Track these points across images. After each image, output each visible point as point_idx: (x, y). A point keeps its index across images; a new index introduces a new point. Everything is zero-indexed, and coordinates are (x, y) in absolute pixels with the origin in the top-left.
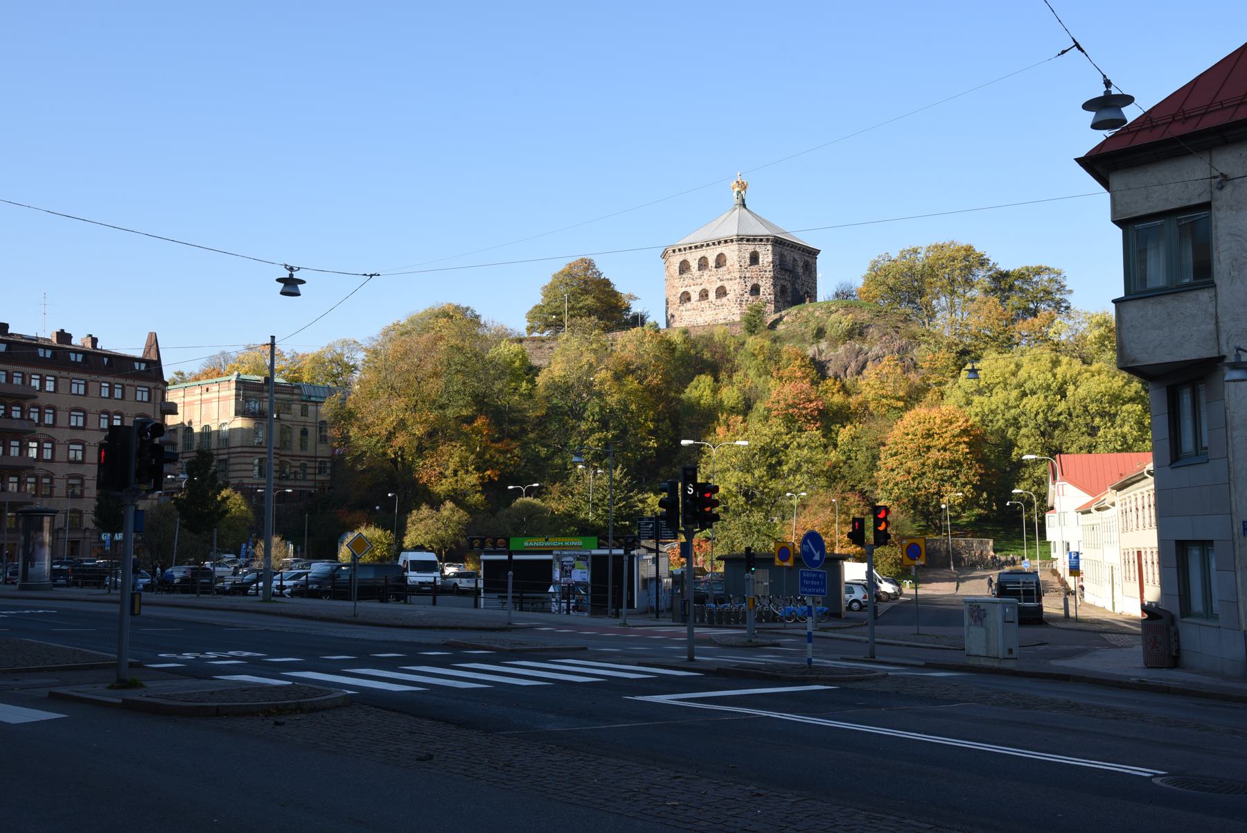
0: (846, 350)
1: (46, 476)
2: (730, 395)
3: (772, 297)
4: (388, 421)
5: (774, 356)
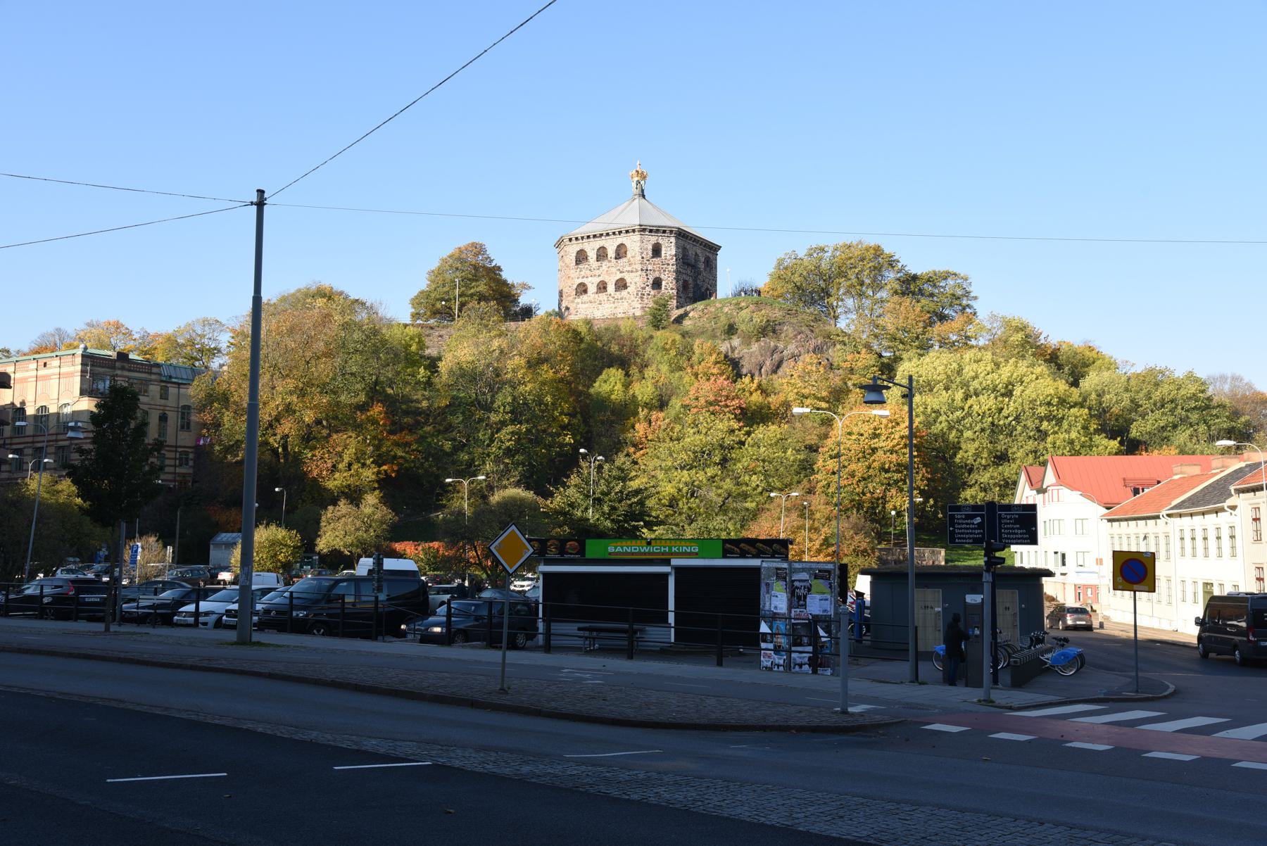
0: (761, 347)
2: (643, 390)
3: (675, 292)
5: (686, 352)
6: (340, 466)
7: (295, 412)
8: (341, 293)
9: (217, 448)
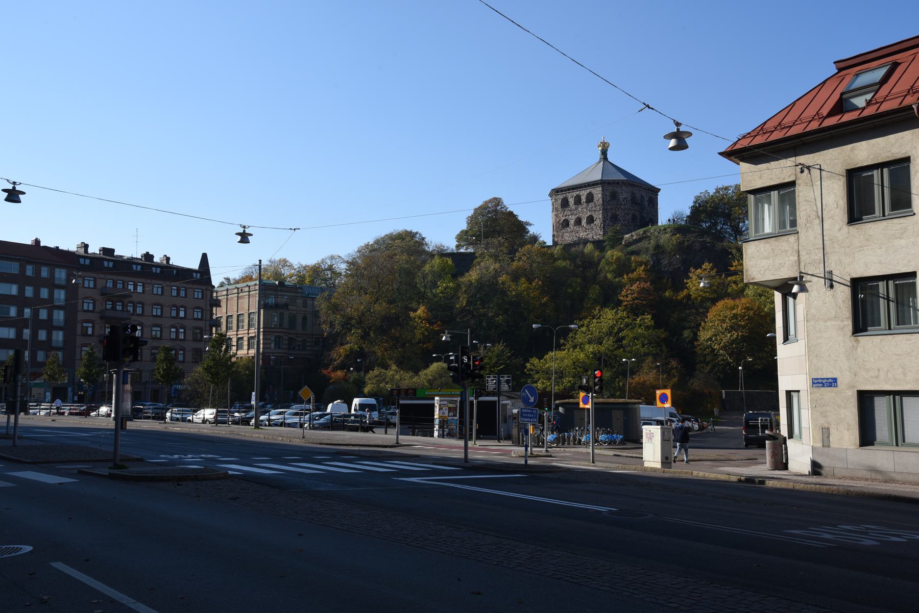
8: (417, 233)
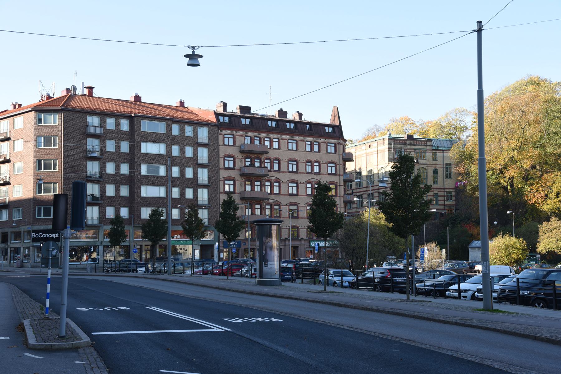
1: (276, 205)
4: (501, 158)
6: (551, 195)
7: (516, 161)
8: (546, 80)
9: (468, 188)
